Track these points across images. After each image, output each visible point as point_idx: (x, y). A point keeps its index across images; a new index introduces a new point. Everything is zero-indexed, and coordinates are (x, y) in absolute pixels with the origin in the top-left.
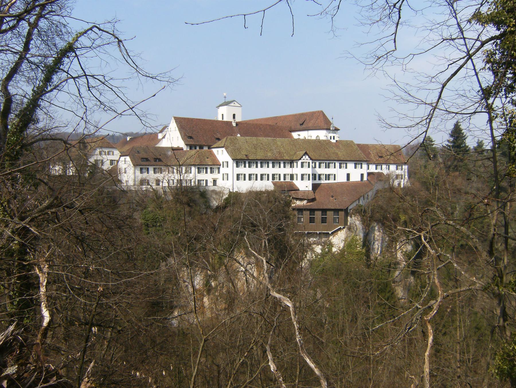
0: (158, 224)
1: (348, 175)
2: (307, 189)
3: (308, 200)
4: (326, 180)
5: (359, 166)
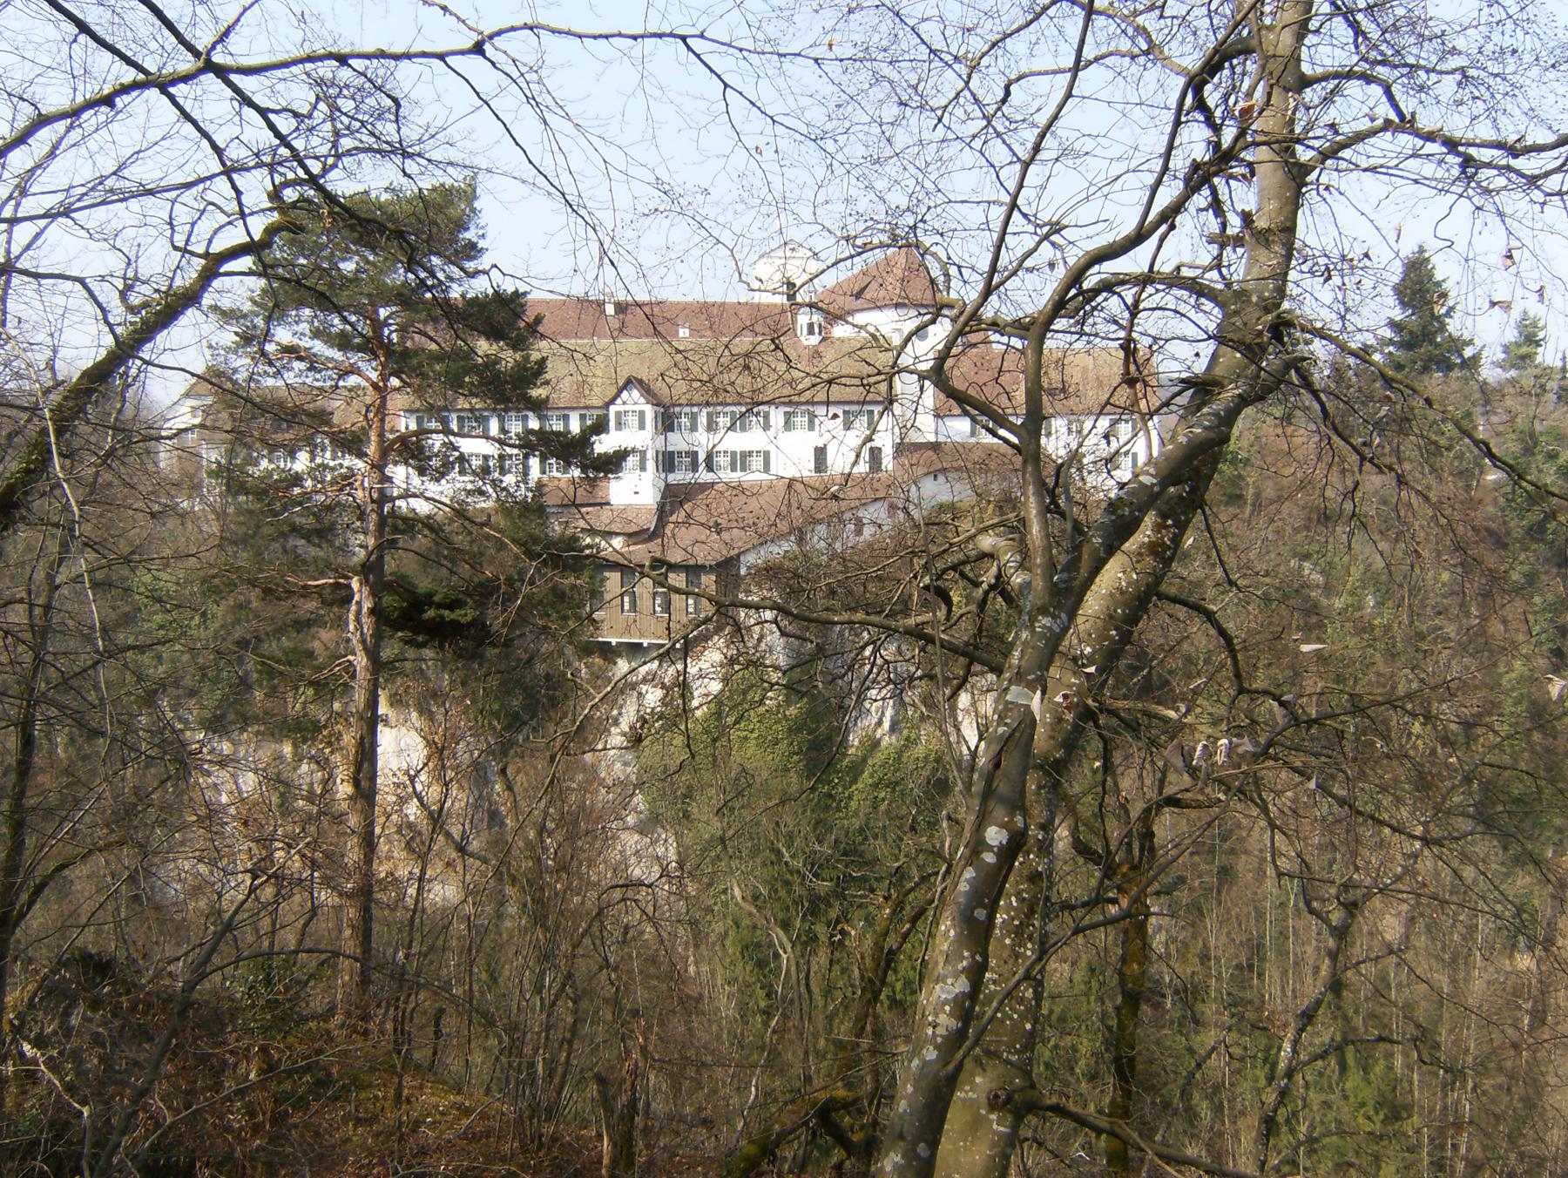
0: (821, 929)
1: (820, 454)
2: (636, 500)
3: (630, 535)
4: (733, 469)
5: (800, 420)
